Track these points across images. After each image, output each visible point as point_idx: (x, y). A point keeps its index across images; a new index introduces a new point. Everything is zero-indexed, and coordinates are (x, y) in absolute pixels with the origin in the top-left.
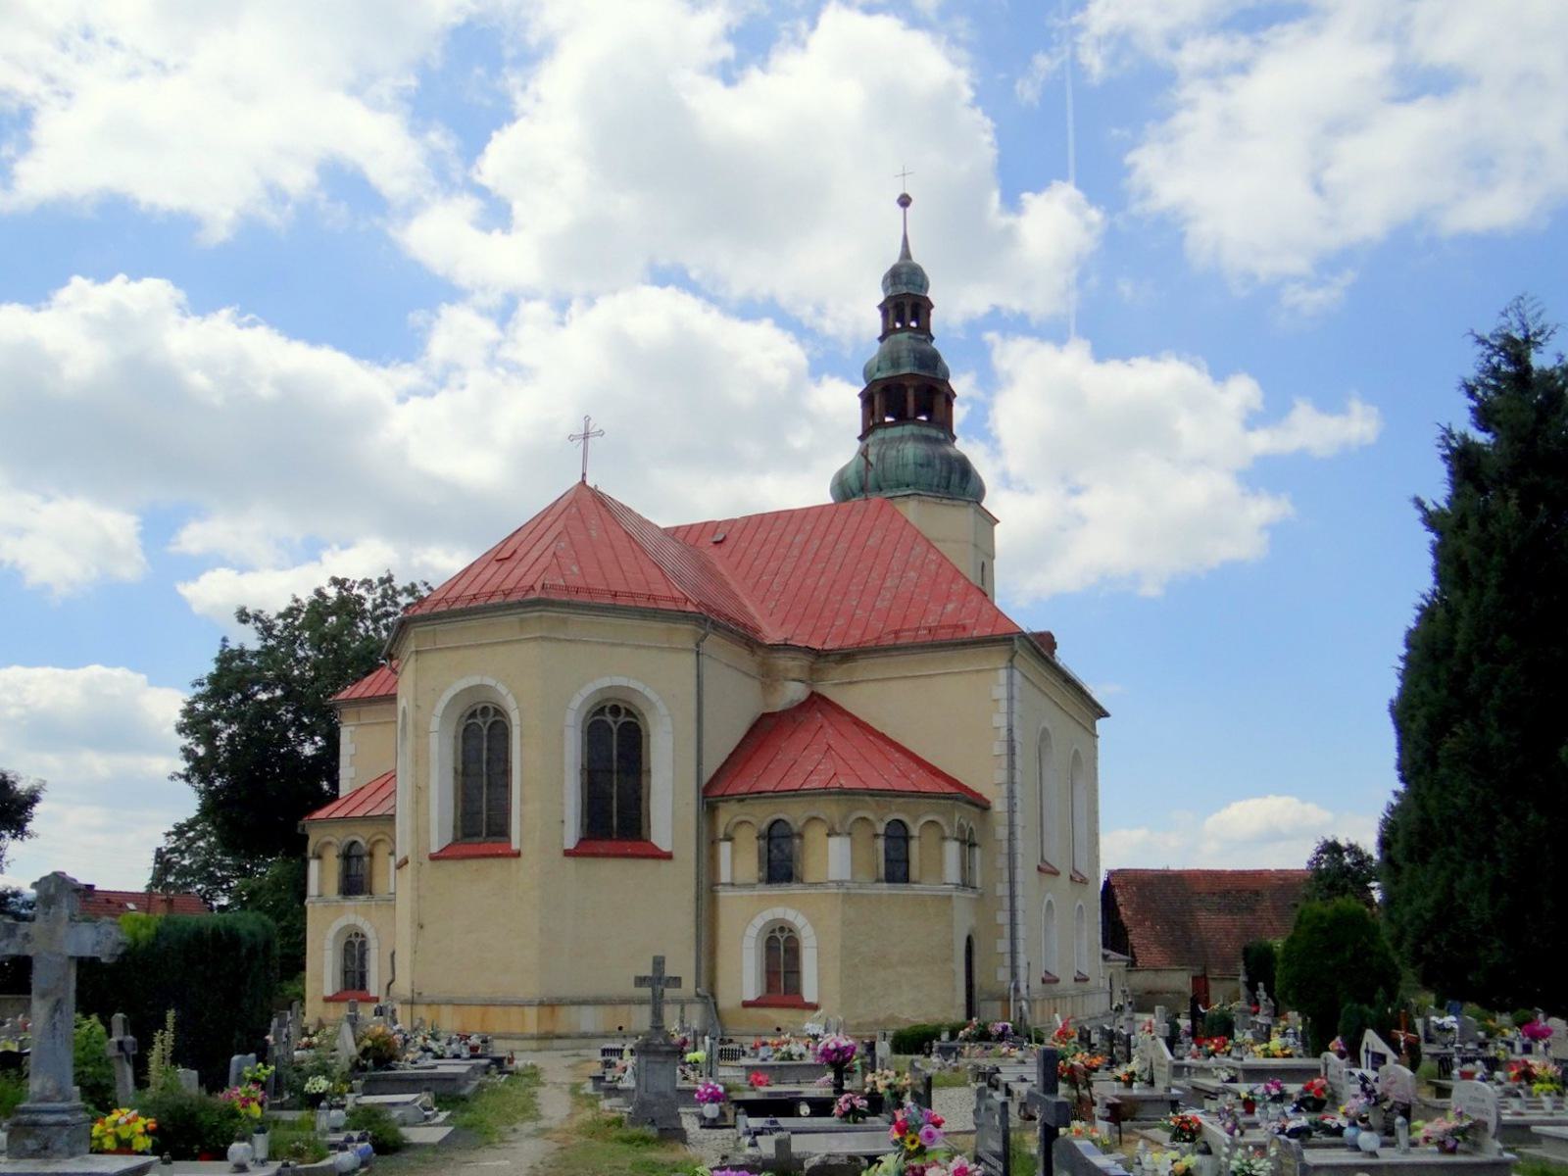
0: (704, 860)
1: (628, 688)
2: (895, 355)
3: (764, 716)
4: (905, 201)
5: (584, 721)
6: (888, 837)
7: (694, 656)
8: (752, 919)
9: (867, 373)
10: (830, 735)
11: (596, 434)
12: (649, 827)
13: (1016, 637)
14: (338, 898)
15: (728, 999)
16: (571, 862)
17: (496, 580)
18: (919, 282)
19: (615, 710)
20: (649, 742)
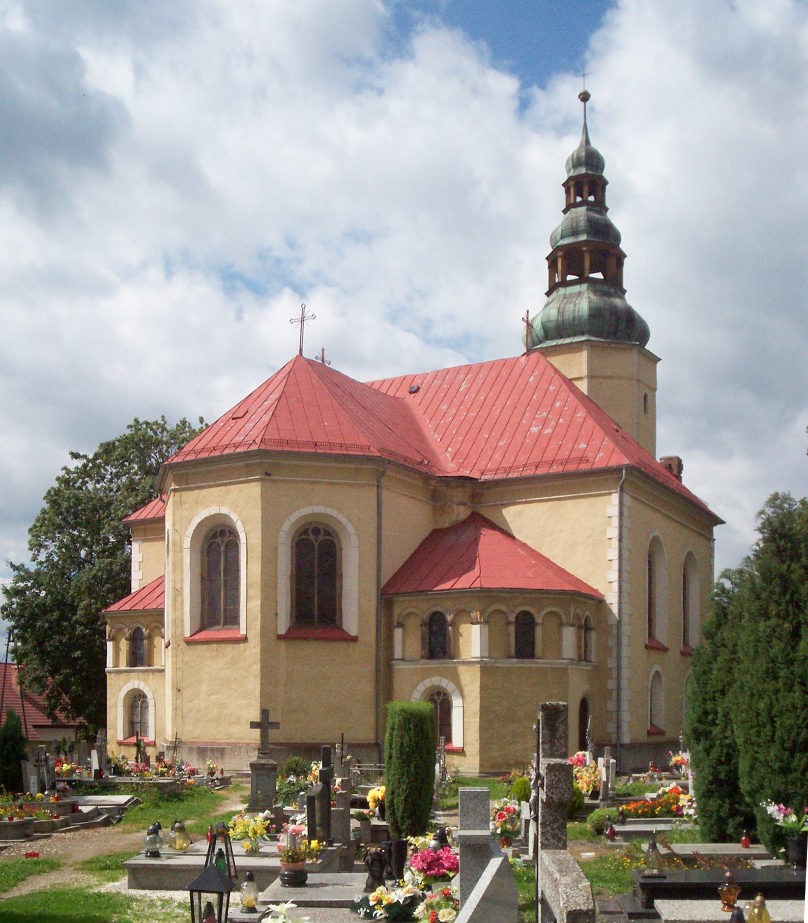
2: (575, 226)
5: (293, 540)
6: (517, 622)
9: (553, 240)
16: (283, 645)
19: (316, 531)
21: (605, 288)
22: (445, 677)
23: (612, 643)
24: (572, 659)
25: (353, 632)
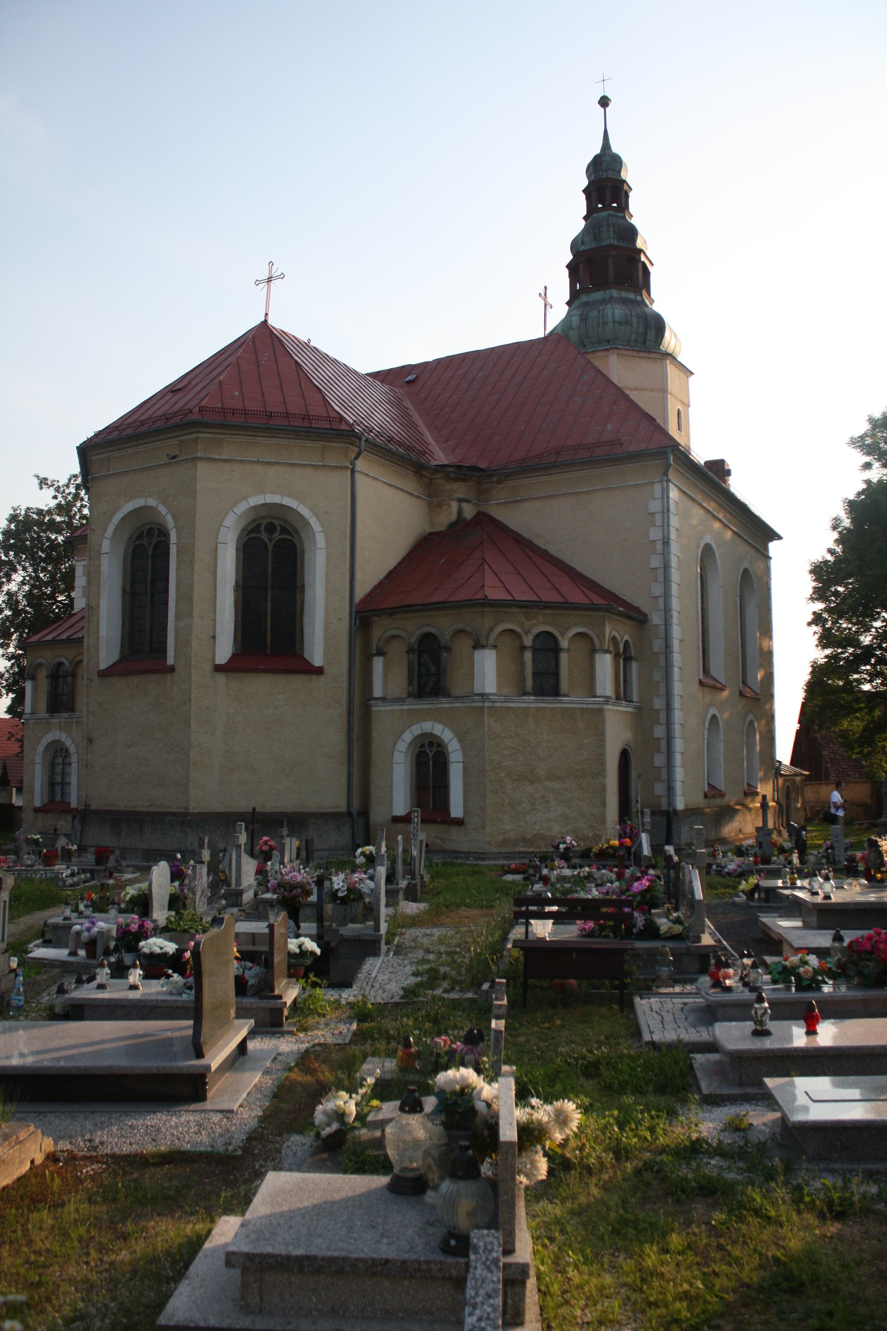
3: (431, 534)
4: (604, 102)
7: (349, 473)
8: (402, 734)
11: (278, 277)
12: (303, 642)
14: (46, 715)
16: (221, 678)
19: (271, 528)
20: (303, 557)
22: (440, 722)
23: (657, 676)
24: (608, 697)
25: (318, 662)
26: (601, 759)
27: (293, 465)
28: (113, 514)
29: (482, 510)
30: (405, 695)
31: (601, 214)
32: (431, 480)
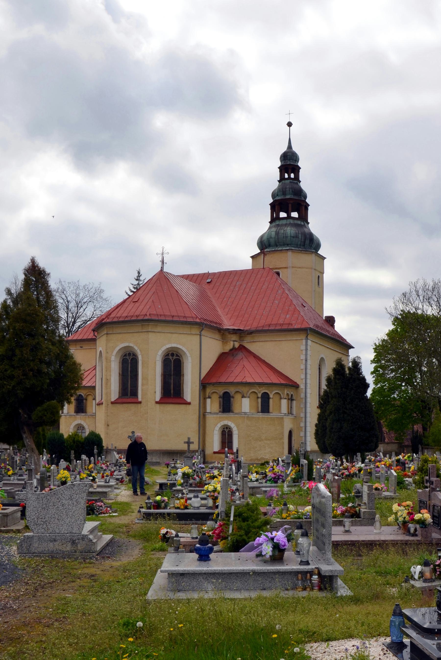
0: (201, 404)
1: (177, 348)
3: (223, 353)
4: (290, 124)
5: (162, 359)
7: (199, 336)
10: (245, 362)
13: (308, 329)
14: (75, 414)
15: (208, 451)
16: (158, 406)
17: (133, 310)
18: (295, 159)
19: (173, 355)
21: (299, 222)
22: (230, 421)
23: (302, 406)
25: (189, 400)
26: (282, 434)
27: (180, 333)
28: (115, 347)
29: (241, 344)
30: (218, 412)
31: (286, 181)
32: (223, 333)
